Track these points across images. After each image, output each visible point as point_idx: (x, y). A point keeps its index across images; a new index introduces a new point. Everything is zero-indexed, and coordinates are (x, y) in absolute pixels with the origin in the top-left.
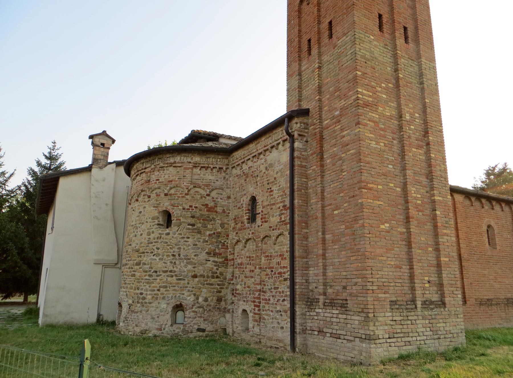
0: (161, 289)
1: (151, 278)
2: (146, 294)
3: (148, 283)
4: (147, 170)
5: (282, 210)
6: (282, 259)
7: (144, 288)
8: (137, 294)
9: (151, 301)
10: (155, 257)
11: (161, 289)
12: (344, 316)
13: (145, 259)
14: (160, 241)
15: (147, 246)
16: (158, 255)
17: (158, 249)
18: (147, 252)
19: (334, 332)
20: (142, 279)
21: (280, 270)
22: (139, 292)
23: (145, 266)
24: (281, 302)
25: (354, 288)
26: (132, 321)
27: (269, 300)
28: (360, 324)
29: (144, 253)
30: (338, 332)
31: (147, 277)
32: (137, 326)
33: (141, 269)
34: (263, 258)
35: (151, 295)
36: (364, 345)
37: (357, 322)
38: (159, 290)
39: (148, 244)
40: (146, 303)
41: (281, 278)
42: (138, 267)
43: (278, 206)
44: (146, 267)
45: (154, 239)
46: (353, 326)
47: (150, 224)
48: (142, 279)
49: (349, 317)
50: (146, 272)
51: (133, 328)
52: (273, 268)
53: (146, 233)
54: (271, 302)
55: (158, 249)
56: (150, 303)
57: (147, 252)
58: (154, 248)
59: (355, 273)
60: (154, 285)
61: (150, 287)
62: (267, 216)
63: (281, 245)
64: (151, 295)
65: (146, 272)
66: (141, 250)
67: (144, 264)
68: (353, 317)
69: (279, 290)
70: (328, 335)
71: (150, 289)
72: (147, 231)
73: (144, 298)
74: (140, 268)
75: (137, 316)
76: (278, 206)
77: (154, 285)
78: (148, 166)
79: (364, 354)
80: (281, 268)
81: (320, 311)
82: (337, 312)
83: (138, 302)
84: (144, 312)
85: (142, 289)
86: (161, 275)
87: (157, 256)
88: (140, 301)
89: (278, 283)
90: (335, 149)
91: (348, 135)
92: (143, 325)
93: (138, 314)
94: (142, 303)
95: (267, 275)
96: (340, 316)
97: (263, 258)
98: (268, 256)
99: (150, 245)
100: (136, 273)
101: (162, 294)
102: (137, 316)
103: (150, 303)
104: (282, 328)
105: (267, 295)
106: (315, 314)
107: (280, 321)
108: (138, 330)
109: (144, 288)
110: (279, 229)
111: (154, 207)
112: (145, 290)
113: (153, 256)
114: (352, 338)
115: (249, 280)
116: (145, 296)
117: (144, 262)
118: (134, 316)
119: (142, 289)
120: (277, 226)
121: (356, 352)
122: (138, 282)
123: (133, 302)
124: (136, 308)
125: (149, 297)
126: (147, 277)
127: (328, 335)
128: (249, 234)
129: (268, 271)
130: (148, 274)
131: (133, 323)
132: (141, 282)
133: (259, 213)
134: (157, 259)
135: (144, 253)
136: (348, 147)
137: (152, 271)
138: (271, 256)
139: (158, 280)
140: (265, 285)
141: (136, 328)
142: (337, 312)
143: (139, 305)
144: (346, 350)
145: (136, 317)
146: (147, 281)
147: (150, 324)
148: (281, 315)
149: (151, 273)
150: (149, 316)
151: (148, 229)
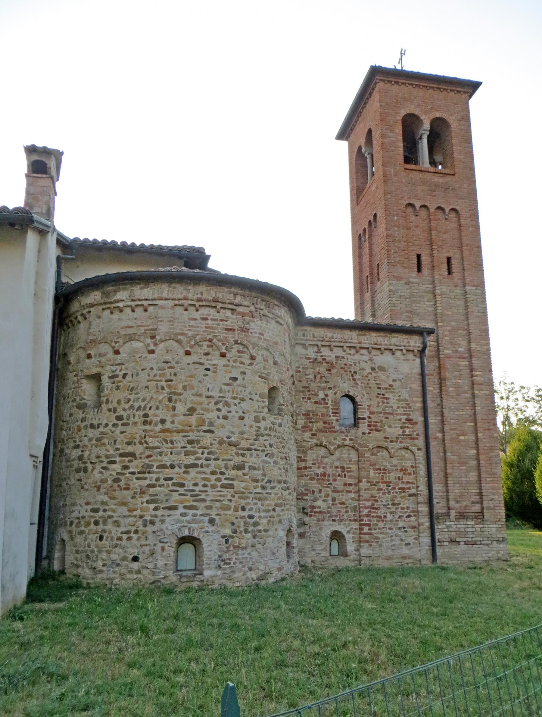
0: (277, 509)
1: (264, 492)
2: (260, 517)
3: (260, 499)
4: (240, 309)
5: (404, 423)
6: (405, 474)
7: (254, 507)
8: (242, 518)
9: (267, 528)
10: (267, 459)
11: (277, 509)
12: (481, 526)
13: (253, 459)
14: (272, 434)
15: (255, 440)
16: (272, 456)
17: (271, 445)
18: (256, 450)
19: (469, 539)
20: (251, 493)
21: (401, 485)
22: (246, 513)
23: (255, 472)
24: (404, 518)
25: (491, 502)
26: (241, 563)
27: (385, 517)
28: (497, 530)
29: (249, 449)
30: (474, 539)
31: (259, 490)
32: (250, 569)
33: (247, 477)
34: (372, 471)
35: (266, 517)
36: (502, 546)
37: (494, 529)
38: (274, 510)
39: (257, 435)
40: (260, 531)
41: (403, 494)
42: (240, 473)
43: (399, 417)
44: (257, 474)
45: (266, 429)
46: (490, 533)
47: (259, 403)
48: (251, 493)
49: (486, 526)
50: (257, 481)
51: (244, 574)
52: (390, 482)
53: (252, 418)
54: (388, 519)
55: (271, 445)
56: (266, 531)
57: (256, 450)
58: (267, 443)
59: (491, 491)
60: (268, 502)
61: (262, 505)
62: (379, 425)
63: (402, 460)
64: (266, 517)
65: (257, 481)
66: (244, 444)
67: (252, 468)
68: (490, 526)
69: (402, 505)
70: (462, 543)
71: (263, 508)
72: (255, 414)
73: (256, 524)
74: (244, 474)
75: (249, 554)
76: (399, 417)
77: (268, 502)
78: (246, 303)
79: (501, 552)
80: (403, 483)
81: (452, 523)
82: (473, 523)
83: (246, 531)
84: (258, 546)
85: (251, 509)
86: (275, 487)
87: (270, 457)
88: (250, 529)
89: (399, 499)
90: (459, 381)
91: (481, 376)
92: (262, 567)
93: (249, 550)
94: (253, 531)
95: (380, 490)
96: (476, 526)
97: (372, 471)
98: (377, 469)
99: (261, 438)
100: (235, 483)
101: (279, 516)
102: (249, 554)
103: (266, 531)
104: (408, 544)
105: (381, 513)
106: (444, 526)
107: (403, 538)
108: (253, 575)
109: (254, 507)
110: (401, 442)
111: (260, 377)
112: (256, 511)
113: (266, 456)
114: (490, 542)
115: (343, 495)
116: (258, 520)
117: (250, 464)
118: (244, 554)
119: (251, 509)
120: (397, 438)
121: (494, 552)
122: (241, 498)
123: (235, 532)
124: (243, 541)
125: (264, 521)
126: (259, 490)
127: (462, 543)
128: (345, 440)
129: (383, 486)
130: (260, 484)
131: (244, 567)
132: (249, 498)
133: (364, 419)
134: (272, 461)
135: (249, 449)
136: (481, 386)
137: (265, 481)
138: (385, 470)
139: (273, 495)
140: (377, 501)
141: (249, 574)
142: (473, 523)
143: (249, 535)
144: (483, 552)
145: (246, 555)
146: (258, 496)
147: (271, 564)
148: (406, 531)
149: (263, 483)
150: (269, 551)
151: (255, 412)
